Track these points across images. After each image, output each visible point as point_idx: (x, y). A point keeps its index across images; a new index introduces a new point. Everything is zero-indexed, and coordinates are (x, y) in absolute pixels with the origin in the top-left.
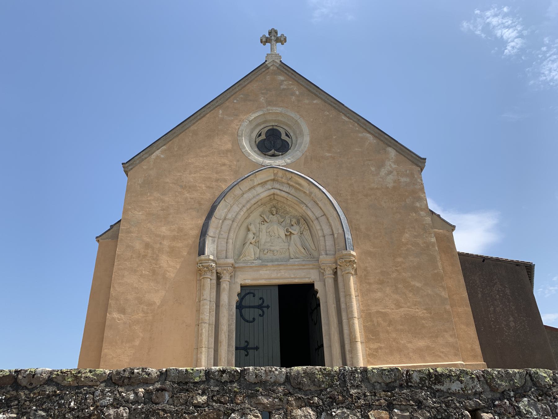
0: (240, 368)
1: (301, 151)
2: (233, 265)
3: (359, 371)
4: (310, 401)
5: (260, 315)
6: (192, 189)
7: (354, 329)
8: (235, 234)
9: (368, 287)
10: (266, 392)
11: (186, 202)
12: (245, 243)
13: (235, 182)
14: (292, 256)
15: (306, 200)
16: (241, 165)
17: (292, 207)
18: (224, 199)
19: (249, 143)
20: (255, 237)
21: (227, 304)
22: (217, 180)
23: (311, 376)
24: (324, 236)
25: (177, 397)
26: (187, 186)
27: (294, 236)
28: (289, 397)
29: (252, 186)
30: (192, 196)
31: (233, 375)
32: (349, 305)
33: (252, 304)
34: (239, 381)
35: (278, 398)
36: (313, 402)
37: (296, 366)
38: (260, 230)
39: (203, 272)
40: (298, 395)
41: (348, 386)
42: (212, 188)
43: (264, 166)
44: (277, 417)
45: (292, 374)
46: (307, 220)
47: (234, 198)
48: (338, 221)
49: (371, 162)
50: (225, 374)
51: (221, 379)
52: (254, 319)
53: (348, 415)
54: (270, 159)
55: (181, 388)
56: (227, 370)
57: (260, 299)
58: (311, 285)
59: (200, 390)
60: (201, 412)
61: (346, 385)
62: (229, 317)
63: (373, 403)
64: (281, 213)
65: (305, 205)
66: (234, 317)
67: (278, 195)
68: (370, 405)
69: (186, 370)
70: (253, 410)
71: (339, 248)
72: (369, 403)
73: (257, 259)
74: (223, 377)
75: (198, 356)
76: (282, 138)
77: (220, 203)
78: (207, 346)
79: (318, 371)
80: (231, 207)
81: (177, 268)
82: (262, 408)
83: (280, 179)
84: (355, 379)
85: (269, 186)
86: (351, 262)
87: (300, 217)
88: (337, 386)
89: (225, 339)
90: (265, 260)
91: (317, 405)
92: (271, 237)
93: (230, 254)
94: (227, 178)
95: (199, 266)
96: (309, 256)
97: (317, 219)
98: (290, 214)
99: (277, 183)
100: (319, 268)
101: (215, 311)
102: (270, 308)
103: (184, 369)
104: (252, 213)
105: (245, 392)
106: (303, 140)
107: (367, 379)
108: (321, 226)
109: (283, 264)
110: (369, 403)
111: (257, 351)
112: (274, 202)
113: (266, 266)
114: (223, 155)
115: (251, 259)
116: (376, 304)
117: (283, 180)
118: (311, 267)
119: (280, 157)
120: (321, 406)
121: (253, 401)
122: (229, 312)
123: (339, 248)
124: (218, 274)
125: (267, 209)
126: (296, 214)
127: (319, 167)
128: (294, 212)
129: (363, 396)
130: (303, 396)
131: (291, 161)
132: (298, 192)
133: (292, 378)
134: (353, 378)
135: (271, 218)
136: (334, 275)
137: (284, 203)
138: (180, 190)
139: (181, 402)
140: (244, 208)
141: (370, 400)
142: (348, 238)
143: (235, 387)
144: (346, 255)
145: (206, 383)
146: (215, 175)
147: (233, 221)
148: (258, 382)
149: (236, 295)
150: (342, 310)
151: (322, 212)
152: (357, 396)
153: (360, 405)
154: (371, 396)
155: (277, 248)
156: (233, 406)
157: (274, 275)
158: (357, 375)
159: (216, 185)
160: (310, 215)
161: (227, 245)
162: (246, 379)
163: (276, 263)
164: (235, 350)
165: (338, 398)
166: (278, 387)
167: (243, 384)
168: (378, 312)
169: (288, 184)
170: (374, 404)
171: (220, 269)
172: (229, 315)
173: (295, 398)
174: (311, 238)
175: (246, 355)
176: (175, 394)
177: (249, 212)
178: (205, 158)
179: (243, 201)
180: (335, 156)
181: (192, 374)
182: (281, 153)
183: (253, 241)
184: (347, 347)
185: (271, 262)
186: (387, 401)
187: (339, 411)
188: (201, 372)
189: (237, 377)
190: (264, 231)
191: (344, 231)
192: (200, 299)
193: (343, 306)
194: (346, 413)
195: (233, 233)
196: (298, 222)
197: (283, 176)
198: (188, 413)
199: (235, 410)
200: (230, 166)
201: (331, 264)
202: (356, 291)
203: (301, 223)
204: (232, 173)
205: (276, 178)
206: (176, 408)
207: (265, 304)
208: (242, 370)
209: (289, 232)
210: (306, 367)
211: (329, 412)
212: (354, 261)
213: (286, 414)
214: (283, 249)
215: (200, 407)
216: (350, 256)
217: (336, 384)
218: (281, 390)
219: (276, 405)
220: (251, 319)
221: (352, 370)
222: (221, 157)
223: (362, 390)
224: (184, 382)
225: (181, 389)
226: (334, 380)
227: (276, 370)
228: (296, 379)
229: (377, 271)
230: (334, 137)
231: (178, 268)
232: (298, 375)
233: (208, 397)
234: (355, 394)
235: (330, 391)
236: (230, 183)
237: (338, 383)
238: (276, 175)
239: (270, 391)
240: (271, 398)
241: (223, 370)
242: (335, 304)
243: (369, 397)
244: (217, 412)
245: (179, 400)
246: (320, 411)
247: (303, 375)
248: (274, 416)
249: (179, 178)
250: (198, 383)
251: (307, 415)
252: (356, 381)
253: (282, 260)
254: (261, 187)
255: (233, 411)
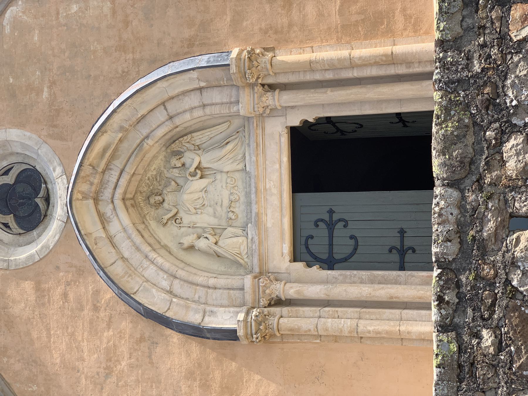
0: (435, 269)
1: (38, 147)
2: (255, 277)
3: (441, 55)
4: (492, 145)
5: (345, 226)
6: (112, 355)
7: (370, 57)
8: (199, 272)
9: (296, 29)
10: (475, 223)
11: (137, 366)
12: (216, 254)
13: (99, 274)
14: (241, 166)
15: (135, 138)
16: (66, 263)
17: (149, 165)
18: (132, 295)
19: (21, 246)
20: (205, 235)
21: (326, 287)
22: (96, 308)
23: (448, 143)
24: (204, 106)
25: (484, 383)
26: (107, 366)
27: (202, 161)
28: (485, 183)
29: (107, 241)
30: (127, 356)
31: (446, 282)
32: (328, 65)
33: (326, 241)
34: (457, 272)
35: (487, 202)
36: (495, 139)
37: (432, 169)
38: (191, 225)
39: (267, 331)
40: (482, 165)
41: (467, 76)
42: (111, 317)
43: (68, 217)
44: (518, 204)
45: (445, 176)
46: (172, 137)
47: (130, 275)
48: (177, 79)
49: (61, 12)
50: (444, 297)
51: (453, 304)
52: (352, 237)
53: (517, 77)
54: (54, 206)
55: (468, 376)
56: (438, 294)
57: (317, 226)
58: (294, 132)
59: (471, 342)
60: (510, 340)
61: (465, 79)
62: (347, 283)
63: (496, 32)
64: (160, 185)
65: (145, 140)
66: (348, 273)
67: (125, 193)
68: (501, 38)
69: (438, 366)
70: (507, 247)
71: (225, 79)
72: (497, 38)
73: (245, 233)
74: (451, 301)
75: (414, 337)
76: (12, 182)
77: (140, 301)
78: (398, 322)
79: (441, 130)
80: (147, 281)
81: (261, 380)
82: (504, 231)
83: (93, 188)
84: (456, 63)
85: (108, 210)
86: (253, 58)
87: (169, 151)
88: (467, 95)
89: (386, 290)
90: (247, 216)
91: (498, 133)
92: (205, 206)
93: (235, 281)
94: (92, 289)
95: (257, 338)
96: (240, 134)
97: (171, 118)
98: (162, 169)
99: (103, 193)
100: (262, 116)
101: (337, 309)
102: (334, 209)
103: (436, 371)
104: (160, 241)
105: (476, 260)
106: (17, 142)
107: (455, 39)
108: (185, 111)
109: (256, 183)
110: (496, 39)
111: (406, 232)
112: (140, 198)
113: (257, 214)
114: (47, 297)
115: (245, 243)
116: (326, 15)
117: (96, 181)
118: (260, 131)
119: (49, 186)
120: (500, 125)
121: (491, 246)
122: (340, 283)
123: (225, 79)
124: (273, 303)
125: (153, 212)
126: (161, 157)
127: (70, 111)
128: (159, 162)
129: (486, 49)
130: (484, 157)
131: (59, 165)
132: (120, 153)
133: (452, 177)
134: (454, 65)
135: (169, 204)
136: (275, 90)
137: (141, 180)
138: (114, 379)
139: (492, 376)
140: (150, 257)
141: (491, 36)
142: (208, 62)
143: (467, 278)
144: (238, 66)
145: (460, 331)
146: (86, 312)
147: (175, 277)
148: (460, 237)
149: (309, 269)
150: (337, 77)
151: (159, 108)
152: (484, 60)
153: (500, 55)
154: (484, 34)
155: (226, 193)
156: (500, 283)
157: (274, 200)
158: (449, 59)
159: (106, 310)
160: (163, 131)
161: (220, 289)
162: (454, 259)
163: (253, 196)
164: (404, 272)
165: (488, 94)
166: (468, 202)
167: (461, 264)
168: (341, 12)
169: (104, 172)
170: (498, 30)
171: (263, 300)
172: (344, 282)
173: (486, 172)
174: (208, 130)
175: (414, 251)
176: (478, 387)
177: (157, 246)
178: (52, 332)
179: (136, 258)
180: (49, 80)
181: (445, 356)
182: (43, 186)
183: (212, 239)
184: (402, 70)
185: (251, 206)
186: (494, 7)
187: (510, 93)
188: (440, 341)
189: (451, 275)
190: (194, 218)
191: (193, 69)
192: (315, 335)
193: (329, 76)
194: (513, 81)
195: (198, 278)
196: (178, 154)
197: (88, 183)
198: (510, 362)
199: (507, 279)
200: (68, 284)
201: (256, 95)
202: (304, 50)
203: (179, 149)
204: (81, 280)
205: (91, 195)
206: (503, 384)
207: (326, 217)
208: (438, 265)
209: (195, 170)
210: (434, 150)
211: (512, 111)
212: (249, 52)
213: (513, 189)
214: (227, 183)
215: (501, 342)
216: (240, 59)
217: (464, 97)
218: (474, 196)
219: (499, 205)
220: (352, 242)
221: (440, 68)
222: (49, 301)
223: (475, 51)
224: (459, 371)
225: (470, 377)
226: (458, 101)
227: (438, 204)
228: (454, 169)
229: (268, 10)
230: (11, 80)
231: (259, 377)
232: (448, 166)
233: (484, 326)
234: (481, 63)
235: (475, 108)
236: (102, 284)
237: (462, 94)
238: (86, 194)
239: (474, 215)
240: (486, 214)
241: (437, 301)
242: (326, 89)
243: (488, 39)
244: (509, 312)
245: (489, 378)
246: (510, 126)
247: (447, 157)
248: (517, 209)
249: (91, 380)
250: (459, 346)
251: (516, 150)
252: (459, 60)
253: (248, 184)
254: (111, 223)
255: (508, 282)
